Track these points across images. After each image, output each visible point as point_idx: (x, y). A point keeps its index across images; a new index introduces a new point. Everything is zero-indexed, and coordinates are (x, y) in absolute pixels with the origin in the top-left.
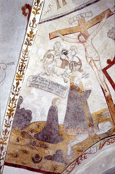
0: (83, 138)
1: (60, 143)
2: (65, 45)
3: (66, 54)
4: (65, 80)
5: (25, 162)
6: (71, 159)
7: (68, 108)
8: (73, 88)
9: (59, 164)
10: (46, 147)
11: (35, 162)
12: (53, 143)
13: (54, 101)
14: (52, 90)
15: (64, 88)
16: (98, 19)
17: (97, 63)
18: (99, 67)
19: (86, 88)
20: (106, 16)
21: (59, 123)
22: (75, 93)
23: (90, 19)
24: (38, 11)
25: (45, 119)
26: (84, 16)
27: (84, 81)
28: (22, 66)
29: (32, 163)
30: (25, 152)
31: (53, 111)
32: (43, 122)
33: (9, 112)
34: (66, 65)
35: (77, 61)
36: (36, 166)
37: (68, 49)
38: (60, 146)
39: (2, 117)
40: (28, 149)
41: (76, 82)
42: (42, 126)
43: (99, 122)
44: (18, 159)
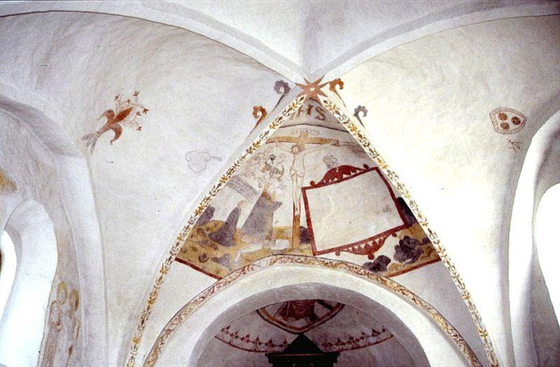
0: (255, 248)
1: (231, 248)
2: (276, 151)
3: (272, 159)
4: (259, 184)
5: (191, 259)
6: (237, 266)
7: (252, 214)
8: (265, 195)
9: (224, 268)
10: (216, 249)
11: (201, 261)
12: (225, 245)
13: (242, 202)
14: (244, 191)
15: (255, 193)
16: (322, 141)
17: (299, 179)
18: (299, 183)
19: (277, 199)
20: (332, 142)
21: (237, 226)
22: (263, 199)
23: (313, 137)
24: (275, 127)
25: (225, 220)
26: (309, 131)
27: (279, 191)
28: (232, 169)
29: (198, 262)
30: (195, 249)
31: (236, 213)
32: (222, 222)
33: (198, 209)
34: (268, 170)
35: (281, 169)
36: (199, 265)
37: (277, 155)
38: (230, 250)
39: (276, 277)
40: (197, 246)
41: (270, 191)
42: (220, 226)
43: (278, 238)
44: (186, 255)
